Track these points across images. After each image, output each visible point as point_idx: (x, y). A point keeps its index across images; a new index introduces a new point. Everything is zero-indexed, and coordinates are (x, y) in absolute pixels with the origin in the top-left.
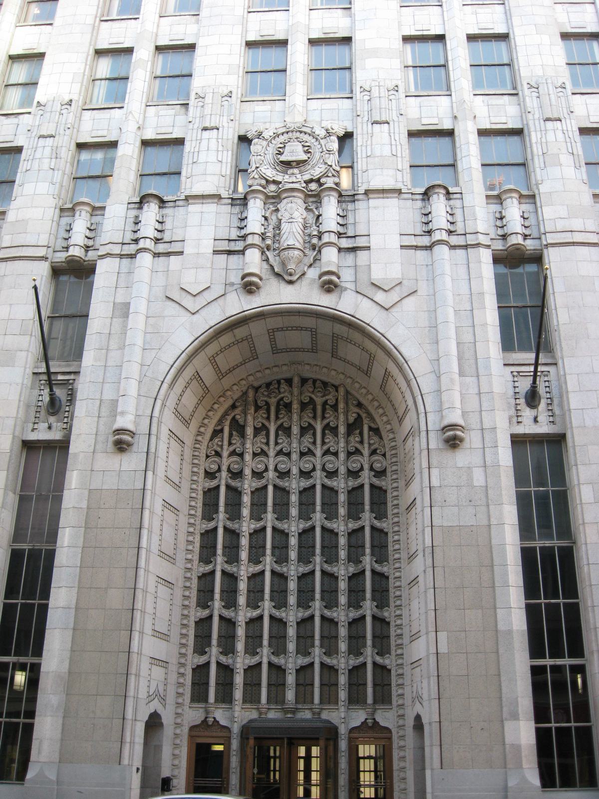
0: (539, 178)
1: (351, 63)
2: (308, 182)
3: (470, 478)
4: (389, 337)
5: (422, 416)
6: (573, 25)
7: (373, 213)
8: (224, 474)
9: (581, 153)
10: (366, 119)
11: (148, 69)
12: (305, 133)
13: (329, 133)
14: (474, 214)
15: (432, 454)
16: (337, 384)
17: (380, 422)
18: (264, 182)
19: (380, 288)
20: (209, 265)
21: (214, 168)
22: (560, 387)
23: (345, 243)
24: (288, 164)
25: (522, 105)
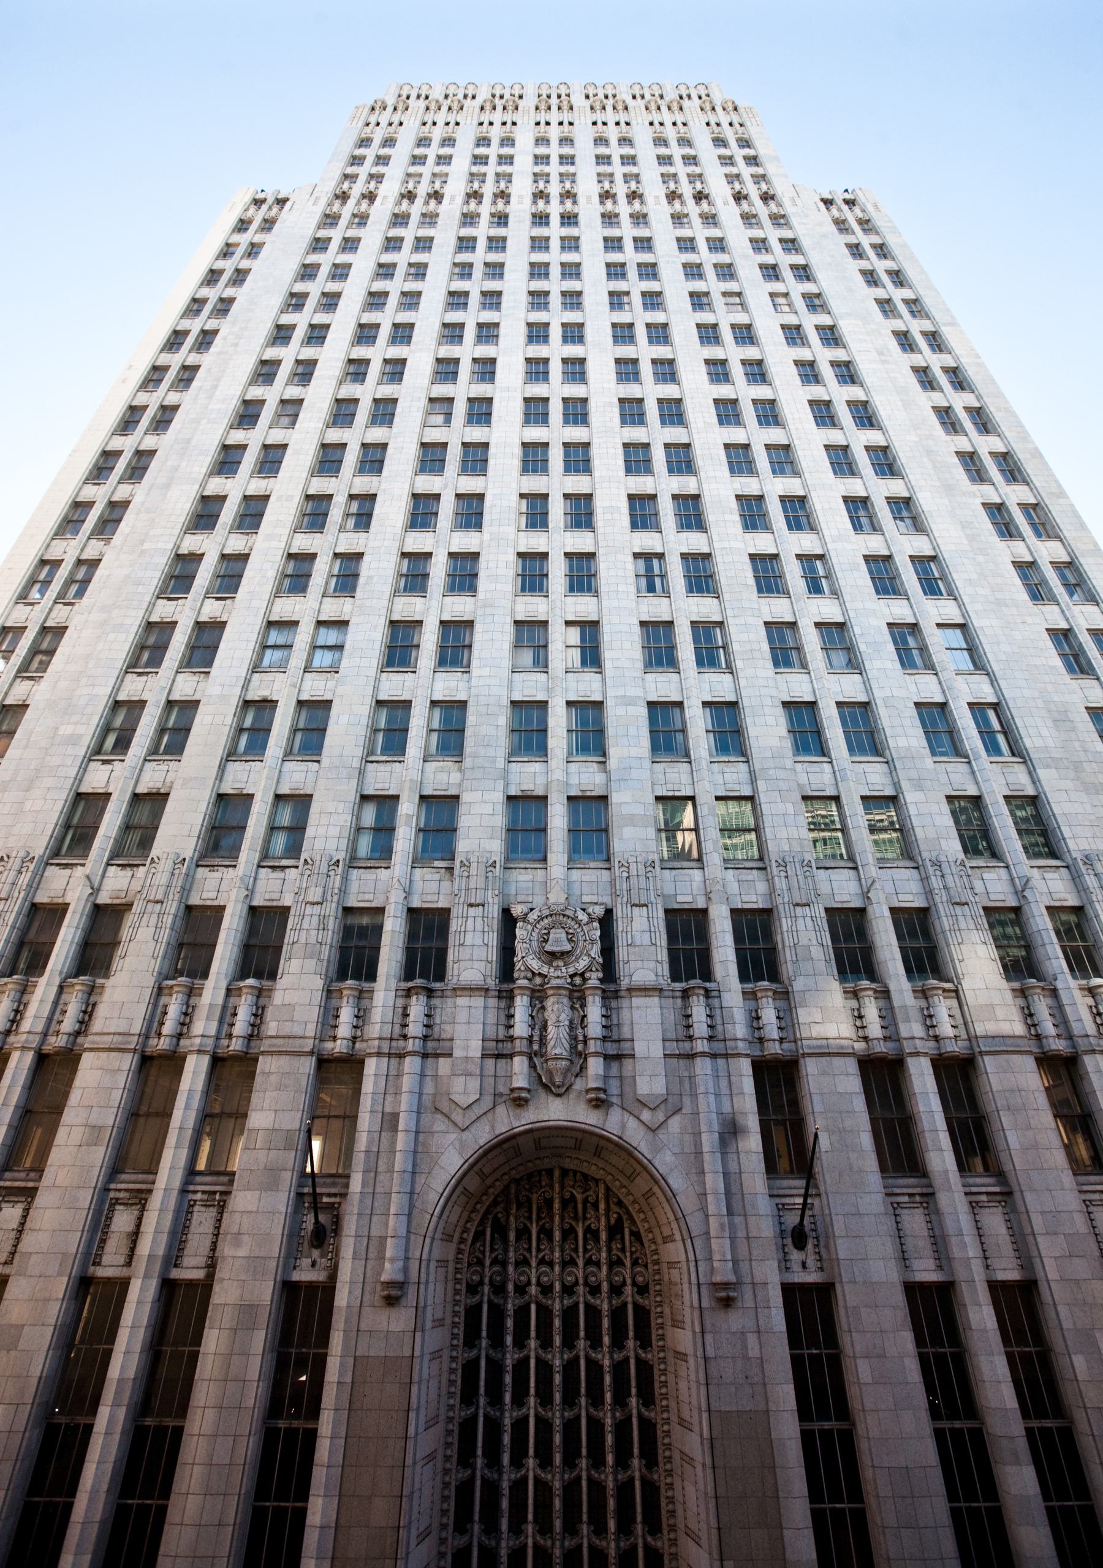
0: (791, 973)
1: (607, 825)
2: (572, 976)
3: (745, 1346)
4: (656, 1164)
5: (692, 1264)
6: (814, 787)
7: (636, 1014)
8: (486, 1289)
9: (830, 943)
10: (625, 899)
11: (414, 825)
12: (569, 917)
14: (732, 1017)
15: (706, 1314)
17: (642, 1227)
19: (645, 1105)
20: (478, 1072)
21: (481, 953)
22: (826, 1233)
24: (553, 955)
25: (770, 881)
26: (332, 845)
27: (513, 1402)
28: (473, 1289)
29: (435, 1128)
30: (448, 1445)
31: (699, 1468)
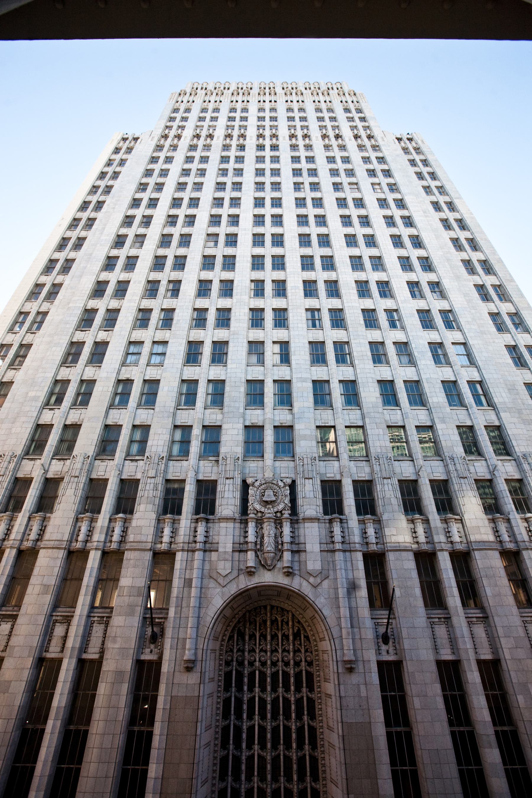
0: (381, 511)
2: (276, 513)
3: (359, 691)
4: (316, 603)
5: (334, 652)
6: (392, 421)
7: (307, 531)
8: (235, 663)
9: (400, 497)
11: (200, 440)
13: (285, 485)
14: (353, 532)
16: (288, 610)
17: (310, 634)
18: (255, 512)
20: (231, 559)
21: (232, 501)
22: (399, 636)
23: (295, 548)
24: (267, 503)
25: (371, 467)
26: (160, 449)
27: (247, 718)
28: (228, 663)
29: (210, 586)
30: (216, 739)
31: (337, 750)
